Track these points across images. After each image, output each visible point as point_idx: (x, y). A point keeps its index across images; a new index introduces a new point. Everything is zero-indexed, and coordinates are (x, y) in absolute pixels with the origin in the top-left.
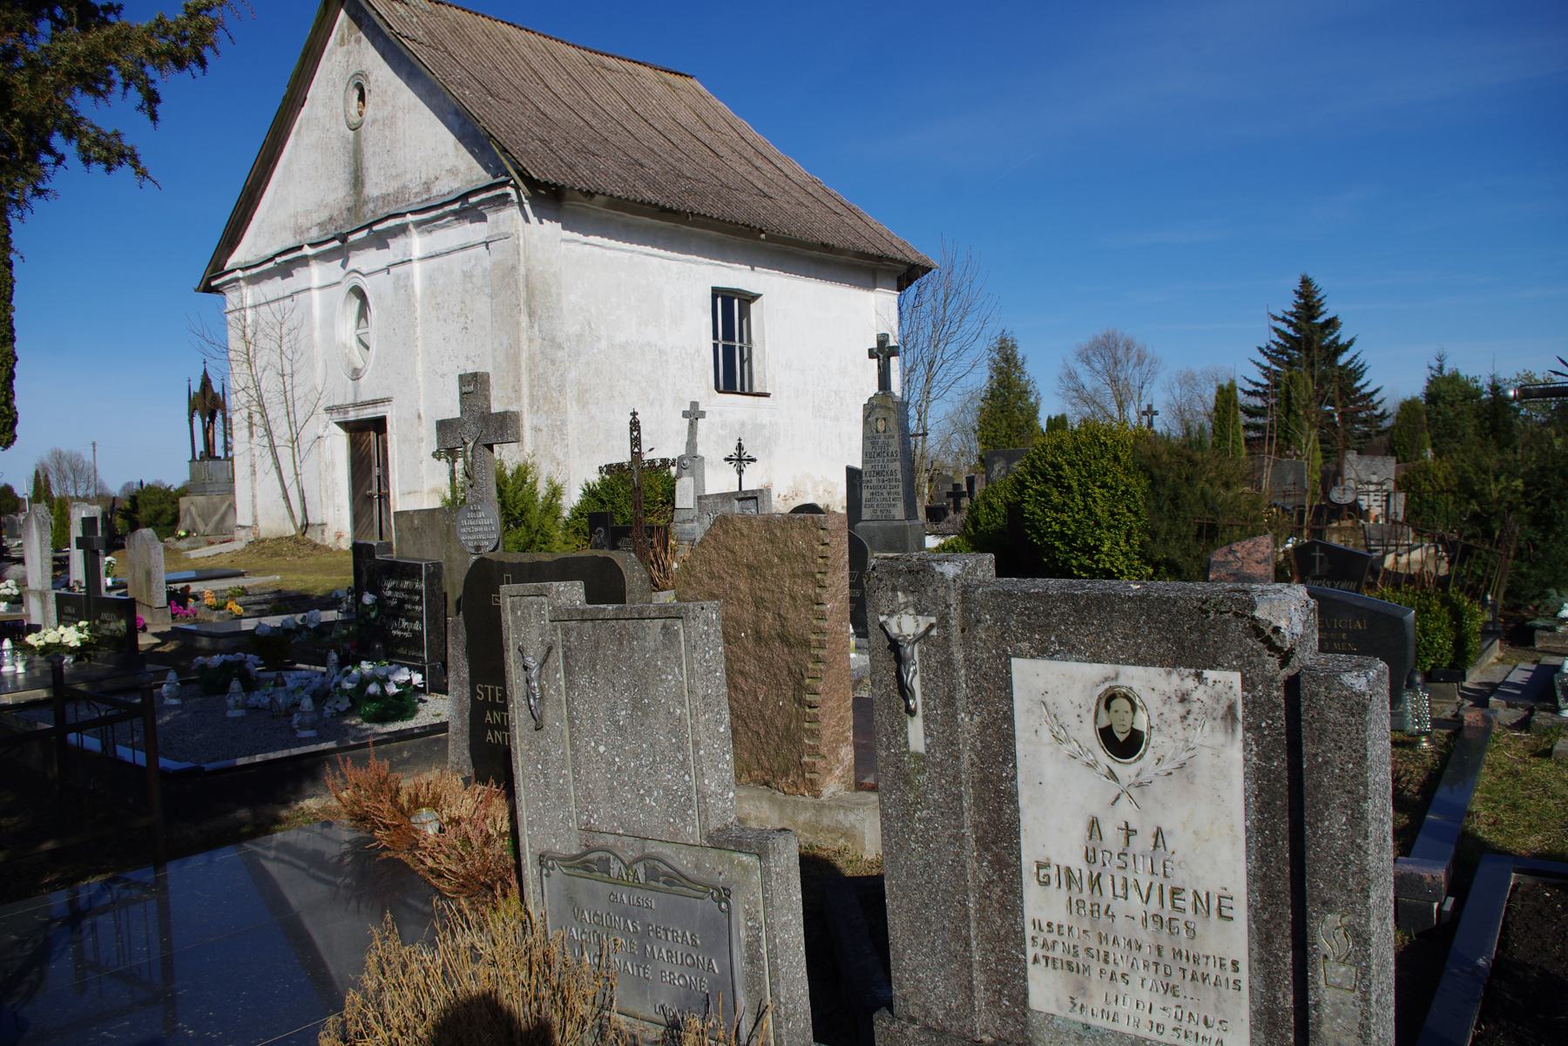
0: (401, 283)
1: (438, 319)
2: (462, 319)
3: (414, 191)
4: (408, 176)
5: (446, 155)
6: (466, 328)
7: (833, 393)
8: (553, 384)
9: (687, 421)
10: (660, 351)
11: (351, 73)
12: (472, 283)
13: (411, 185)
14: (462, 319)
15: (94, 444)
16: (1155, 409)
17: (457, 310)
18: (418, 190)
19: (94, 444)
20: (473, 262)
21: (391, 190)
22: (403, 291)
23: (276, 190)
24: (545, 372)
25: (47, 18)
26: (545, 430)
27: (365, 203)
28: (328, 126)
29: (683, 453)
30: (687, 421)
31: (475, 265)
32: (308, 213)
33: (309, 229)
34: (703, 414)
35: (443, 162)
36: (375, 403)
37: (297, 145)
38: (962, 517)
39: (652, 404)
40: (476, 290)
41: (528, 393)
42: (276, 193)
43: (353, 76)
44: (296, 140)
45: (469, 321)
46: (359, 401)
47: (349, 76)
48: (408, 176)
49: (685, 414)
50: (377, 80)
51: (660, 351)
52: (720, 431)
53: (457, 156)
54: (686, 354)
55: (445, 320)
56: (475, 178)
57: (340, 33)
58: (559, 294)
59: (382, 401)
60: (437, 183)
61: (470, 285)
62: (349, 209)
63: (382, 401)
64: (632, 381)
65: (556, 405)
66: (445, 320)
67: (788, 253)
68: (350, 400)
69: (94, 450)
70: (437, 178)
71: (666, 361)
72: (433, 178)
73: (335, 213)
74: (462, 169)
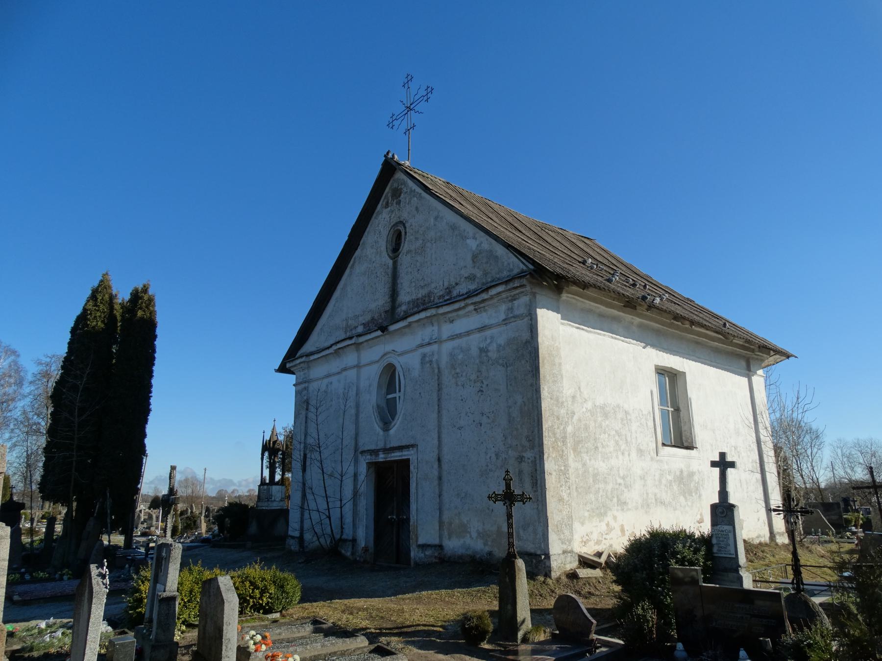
0: (427, 359)
1: (457, 385)
2: (479, 384)
3: (438, 294)
4: (433, 286)
5: (465, 267)
6: (482, 391)
7: (733, 448)
8: (558, 435)
9: (717, 471)
10: (626, 412)
11: (392, 224)
12: (487, 356)
13: (436, 291)
14: (479, 384)
15: (205, 470)
16: (717, 458)
17: (473, 377)
18: (441, 293)
19: (205, 470)
20: (489, 341)
21: (420, 296)
22: (428, 365)
23: (335, 304)
24: (552, 426)
25: (150, 529)
26: (554, 473)
27: (400, 305)
28: (374, 259)
29: (717, 501)
30: (717, 471)
31: (491, 342)
32: (357, 317)
33: (356, 327)
34: (732, 465)
35: (463, 272)
36: (401, 448)
37: (351, 274)
38: (810, 545)
39: (623, 454)
40: (490, 362)
41: (771, 445)
42: (334, 306)
43: (392, 227)
44: (351, 271)
45: (484, 386)
46: (388, 447)
47: (391, 226)
48: (433, 286)
49: (714, 464)
50: (411, 225)
51: (626, 412)
52: (668, 476)
53: (474, 267)
54: (642, 415)
55: (463, 386)
56: (489, 280)
57: (386, 200)
58: (560, 364)
59: (407, 447)
60: (457, 287)
61: (485, 358)
62: (386, 312)
63: (407, 447)
64: (609, 435)
65: (561, 453)
66: (463, 386)
67: (697, 343)
68: (381, 445)
69: (205, 473)
70: (457, 284)
71: (630, 420)
72: (454, 284)
73: (376, 317)
74: (478, 275)
